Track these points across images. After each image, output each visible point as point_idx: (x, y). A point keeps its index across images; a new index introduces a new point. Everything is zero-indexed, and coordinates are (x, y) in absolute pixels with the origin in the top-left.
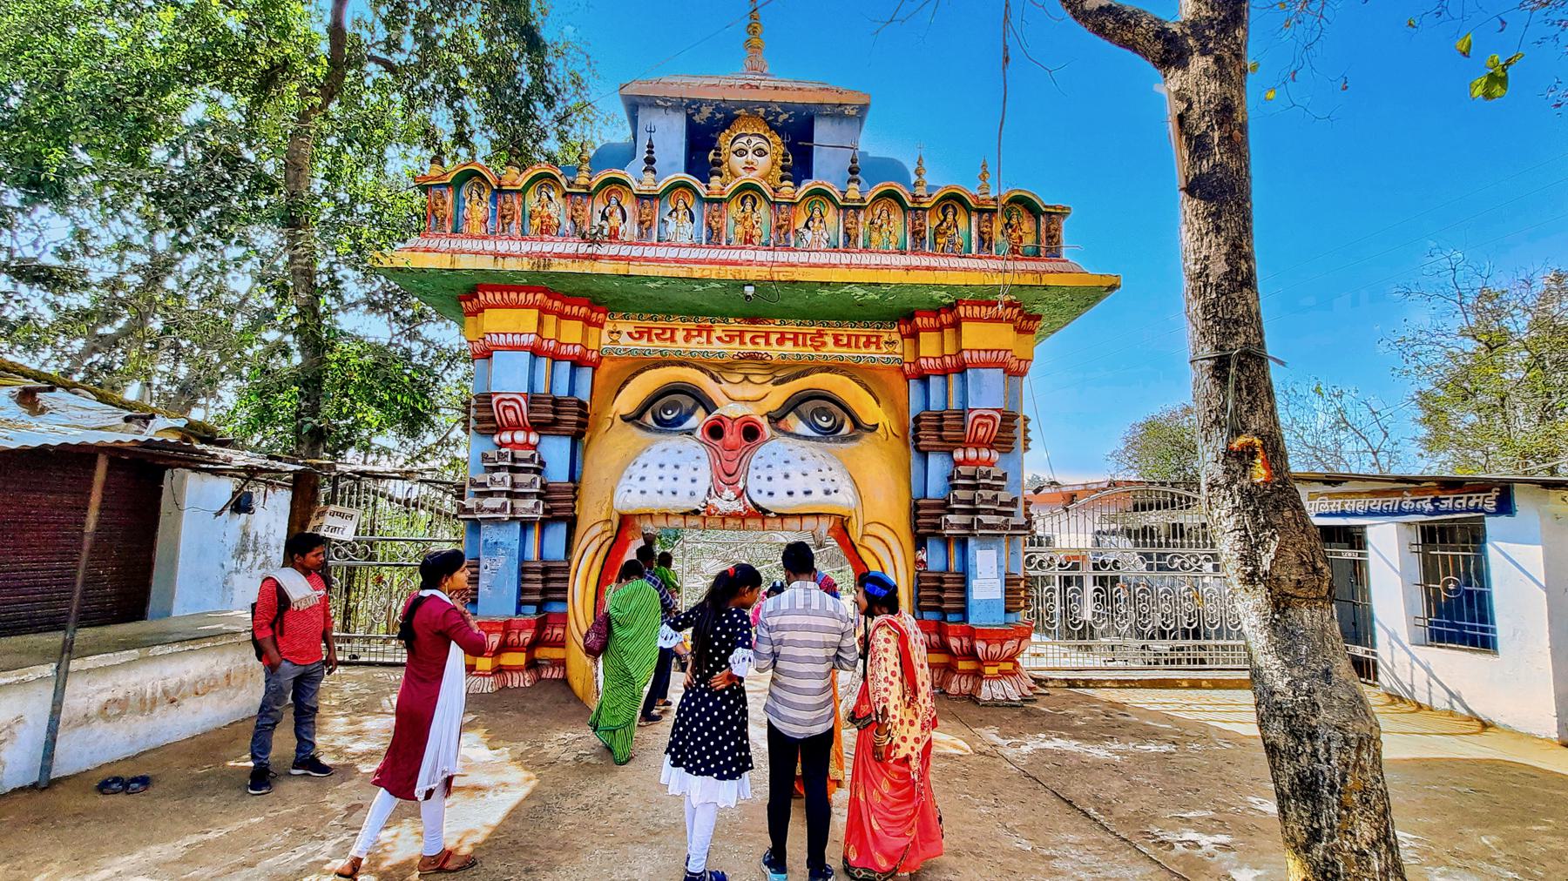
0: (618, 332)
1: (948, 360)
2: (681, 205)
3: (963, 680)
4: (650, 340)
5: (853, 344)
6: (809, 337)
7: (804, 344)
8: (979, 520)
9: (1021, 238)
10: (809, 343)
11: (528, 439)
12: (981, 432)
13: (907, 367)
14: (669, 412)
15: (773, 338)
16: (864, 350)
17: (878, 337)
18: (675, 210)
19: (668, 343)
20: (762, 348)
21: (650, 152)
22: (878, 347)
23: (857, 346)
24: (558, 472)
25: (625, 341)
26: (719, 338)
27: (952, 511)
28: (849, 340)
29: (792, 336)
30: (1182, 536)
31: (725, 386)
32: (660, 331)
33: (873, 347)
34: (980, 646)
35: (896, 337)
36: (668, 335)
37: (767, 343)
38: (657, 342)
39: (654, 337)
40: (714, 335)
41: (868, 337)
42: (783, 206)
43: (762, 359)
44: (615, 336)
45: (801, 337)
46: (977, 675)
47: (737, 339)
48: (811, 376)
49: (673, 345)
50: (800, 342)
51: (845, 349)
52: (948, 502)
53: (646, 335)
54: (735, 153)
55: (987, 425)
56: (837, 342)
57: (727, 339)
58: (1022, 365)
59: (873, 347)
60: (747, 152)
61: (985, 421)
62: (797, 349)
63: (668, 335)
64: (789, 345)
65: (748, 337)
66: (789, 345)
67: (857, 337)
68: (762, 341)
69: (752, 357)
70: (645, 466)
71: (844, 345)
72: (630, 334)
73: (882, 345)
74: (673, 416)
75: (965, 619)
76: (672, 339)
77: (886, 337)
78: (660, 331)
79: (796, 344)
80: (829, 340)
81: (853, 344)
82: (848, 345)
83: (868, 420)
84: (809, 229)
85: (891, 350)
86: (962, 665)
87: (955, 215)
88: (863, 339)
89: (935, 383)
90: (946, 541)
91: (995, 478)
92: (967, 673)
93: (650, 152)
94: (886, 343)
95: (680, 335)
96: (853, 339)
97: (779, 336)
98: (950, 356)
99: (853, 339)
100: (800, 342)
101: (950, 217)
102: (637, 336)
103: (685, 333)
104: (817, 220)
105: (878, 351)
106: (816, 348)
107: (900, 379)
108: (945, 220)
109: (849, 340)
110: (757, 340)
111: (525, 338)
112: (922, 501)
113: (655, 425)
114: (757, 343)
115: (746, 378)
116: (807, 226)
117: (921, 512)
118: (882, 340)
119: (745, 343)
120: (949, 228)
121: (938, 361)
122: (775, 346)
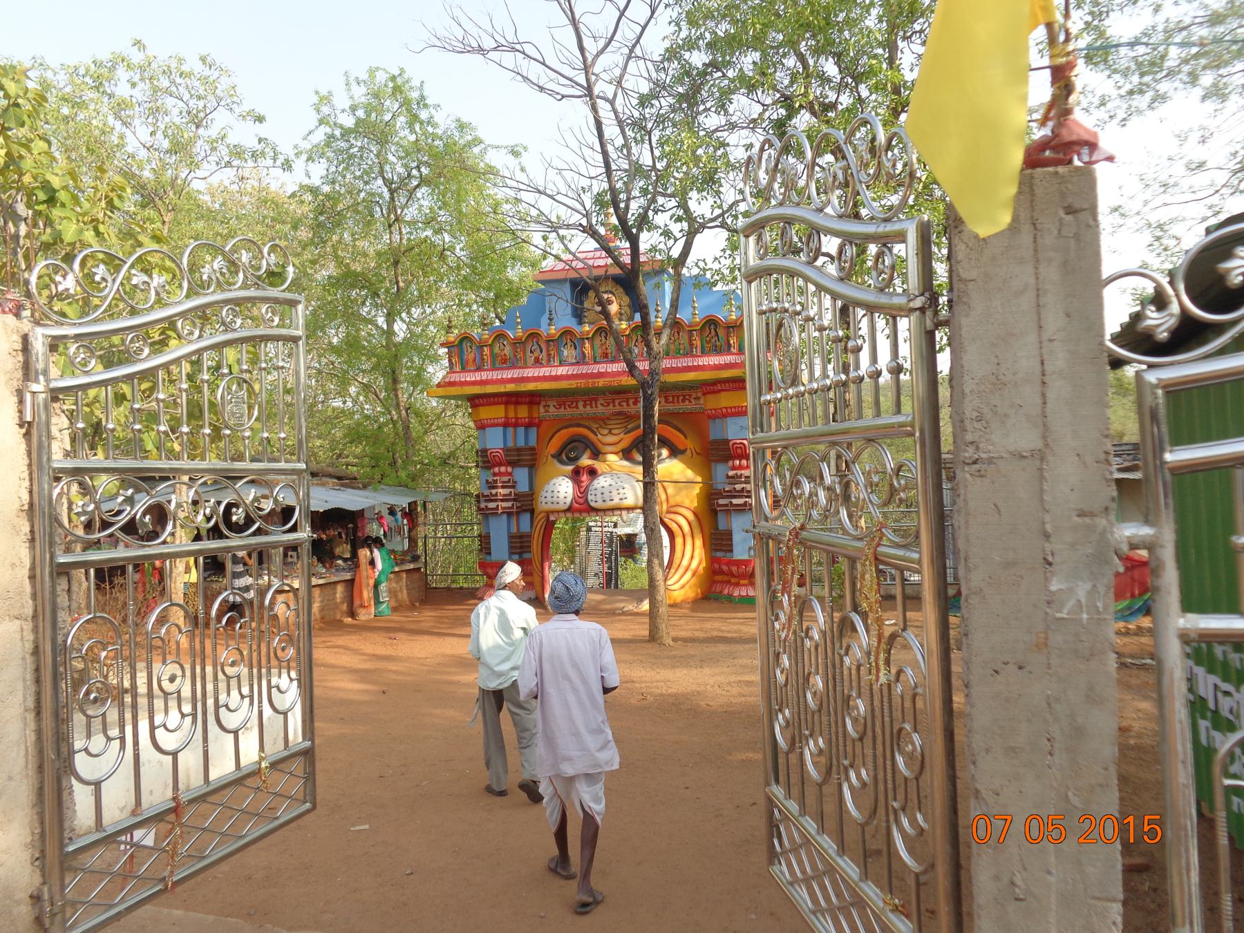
22: (690, 402)
23: (678, 402)
25: (552, 409)
31: (599, 436)
33: (687, 402)
35: (700, 395)
37: (628, 405)
40: (599, 403)
41: (684, 396)
59: (687, 402)
65: (617, 402)
67: (678, 397)
68: (625, 404)
76: (577, 407)
77: (694, 396)
82: (673, 402)
88: (681, 398)
95: (581, 404)
115: (610, 432)
122: (632, 406)
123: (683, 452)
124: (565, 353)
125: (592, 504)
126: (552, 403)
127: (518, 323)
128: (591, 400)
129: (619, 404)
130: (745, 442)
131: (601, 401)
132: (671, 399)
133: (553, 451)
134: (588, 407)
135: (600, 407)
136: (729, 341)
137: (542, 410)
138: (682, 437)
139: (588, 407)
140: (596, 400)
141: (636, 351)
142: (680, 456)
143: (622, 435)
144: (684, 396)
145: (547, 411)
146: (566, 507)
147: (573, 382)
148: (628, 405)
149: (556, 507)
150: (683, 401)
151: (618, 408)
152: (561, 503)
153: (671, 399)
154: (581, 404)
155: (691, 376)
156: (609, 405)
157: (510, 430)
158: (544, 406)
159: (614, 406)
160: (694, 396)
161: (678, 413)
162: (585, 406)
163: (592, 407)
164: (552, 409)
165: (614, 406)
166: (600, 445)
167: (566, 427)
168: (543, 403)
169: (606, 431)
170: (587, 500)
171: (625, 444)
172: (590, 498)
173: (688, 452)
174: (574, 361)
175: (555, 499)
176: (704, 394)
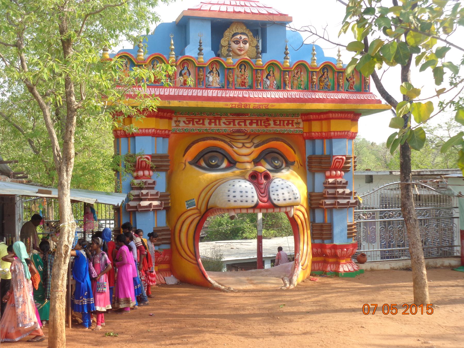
0: (179, 121)
1: (324, 134)
2: (215, 69)
3: (332, 266)
4: (193, 124)
5: (282, 124)
6: (263, 121)
7: (261, 125)
8: (338, 202)
9: (354, 82)
10: (263, 124)
11: (144, 172)
12: (337, 164)
13: (305, 134)
14: (213, 161)
15: (248, 122)
16: (286, 127)
17: (293, 121)
18: (212, 71)
19: (201, 126)
20: (243, 127)
21: (200, 46)
22: (293, 125)
23: (284, 125)
24: (161, 187)
25: (182, 124)
26: (224, 123)
27: (326, 198)
28: (280, 123)
29: (255, 121)
30: (419, 200)
31: (235, 149)
32: (198, 120)
33: (290, 126)
34: (339, 251)
35: (300, 120)
36: (201, 122)
37: (245, 125)
38: (196, 125)
39: (195, 123)
40: (222, 121)
41: (288, 121)
42: (259, 71)
43: (244, 132)
44: (177, 123)
45: (259, 122)
46: (338, 264)
47: (232, 123)
48: (269, 143)
49: (204, 126)
50: (259, 124)
51: (278, 127)
52: (325, 194)
53: (191, 122)
54: (234, 42)
55: (340, 162)
56: (275, 124)
57: (228, 123)
58: (353, 135)
59: (290, 126)
60: (240, 42)
61: (339, 160)
62: (258, 127)
63: (201, 122)
64: (254, 125)
65: (236, 122)
66: (254, 125)
67: (284, 121)
68: (243, 124)
69: (239, 131)
70: (252, 193)
71: (278, 125)
72: (184, 122)
73: (294, 124)
74: (216, 163)
75: (332, 242)
76: (203, 124)
77: (295, 121)
78: (198, 120)
79: (257, 125)
80: (272, 122)
81: (282, 124)
82: (280, 125)
83: (291, 160)
84: (268, 79)
85: (298, 126)
86: (331, 260)
87: (327, 72)
88: (286, 122)
89: (318, 142)
90: (324, 210)
91: (344, 184)
92: (334, 263)
93: (200, 46)
94: (296, 123)
95: (207, 122)
96: (282, 122)
97: (250, 121)
98: (325, 132)
99: (282, 122)
100: (259, 124)
101: (326, 74)
102: (187, 122)
103: (209, 121)
104: (272, 75)
105: (293, 127)
106: (266, 127)
107: (301, 139)
108: (323, 75)
109: (280, 123)
110: (241, 123)
111: (150, 131)
112: (313, 194)
113: (206, 167)
114: (241, 125)
115: (244, 146)
116: (267, 77)
117: (313, 198)
118: (294, 122)
119: (235, 125)
120: (325, 79)
121: (320, 134)
122: (248, 126)
123: (293, 163)
124: (211, 79)
125: (276, 202)
126: (182, 119)
127: (172, 50)
128: (215, 119)
129: (239, 124)
130: (344, 158)
131: (223, 120)
132: (278, 123)
133: (189, 159)
134: (213, 124)
135: (223, 125)
136: (339, 82)
137: (173, 124)
138: (293, 152)
139: (213, 124)
140: (220, 119)
141: (268, 83)
142: (291, 167)
143: (253, 148)
144: (288, 121)
145: (178, 126)
146: (253, 205)
147: (229, 103)
148: (245, 125)
149: (245, 204)
150: (288, 124)
151: (237, 127)
152: (250, 201)
153: (278, 123)
154: (207, 122)
155: (221, 105)
156: (230, 124)
157: (326, 141)
158: (176, 121)
159: (234, 125)
160: (295, 121)
161: (283, 134)
162: (210, 124)
163: (216, 125)
164: (182, 124)
165: (234, 125)
166: (236, 156)
167: (204, 139)
168: (175, 119)
169: (240, 145)
170: (269, 199)
171: (253, 156)
172: (273, 197)
173: (296, 163)
174: (218, 86)
175: (244, 198)
176: (303, 121)
